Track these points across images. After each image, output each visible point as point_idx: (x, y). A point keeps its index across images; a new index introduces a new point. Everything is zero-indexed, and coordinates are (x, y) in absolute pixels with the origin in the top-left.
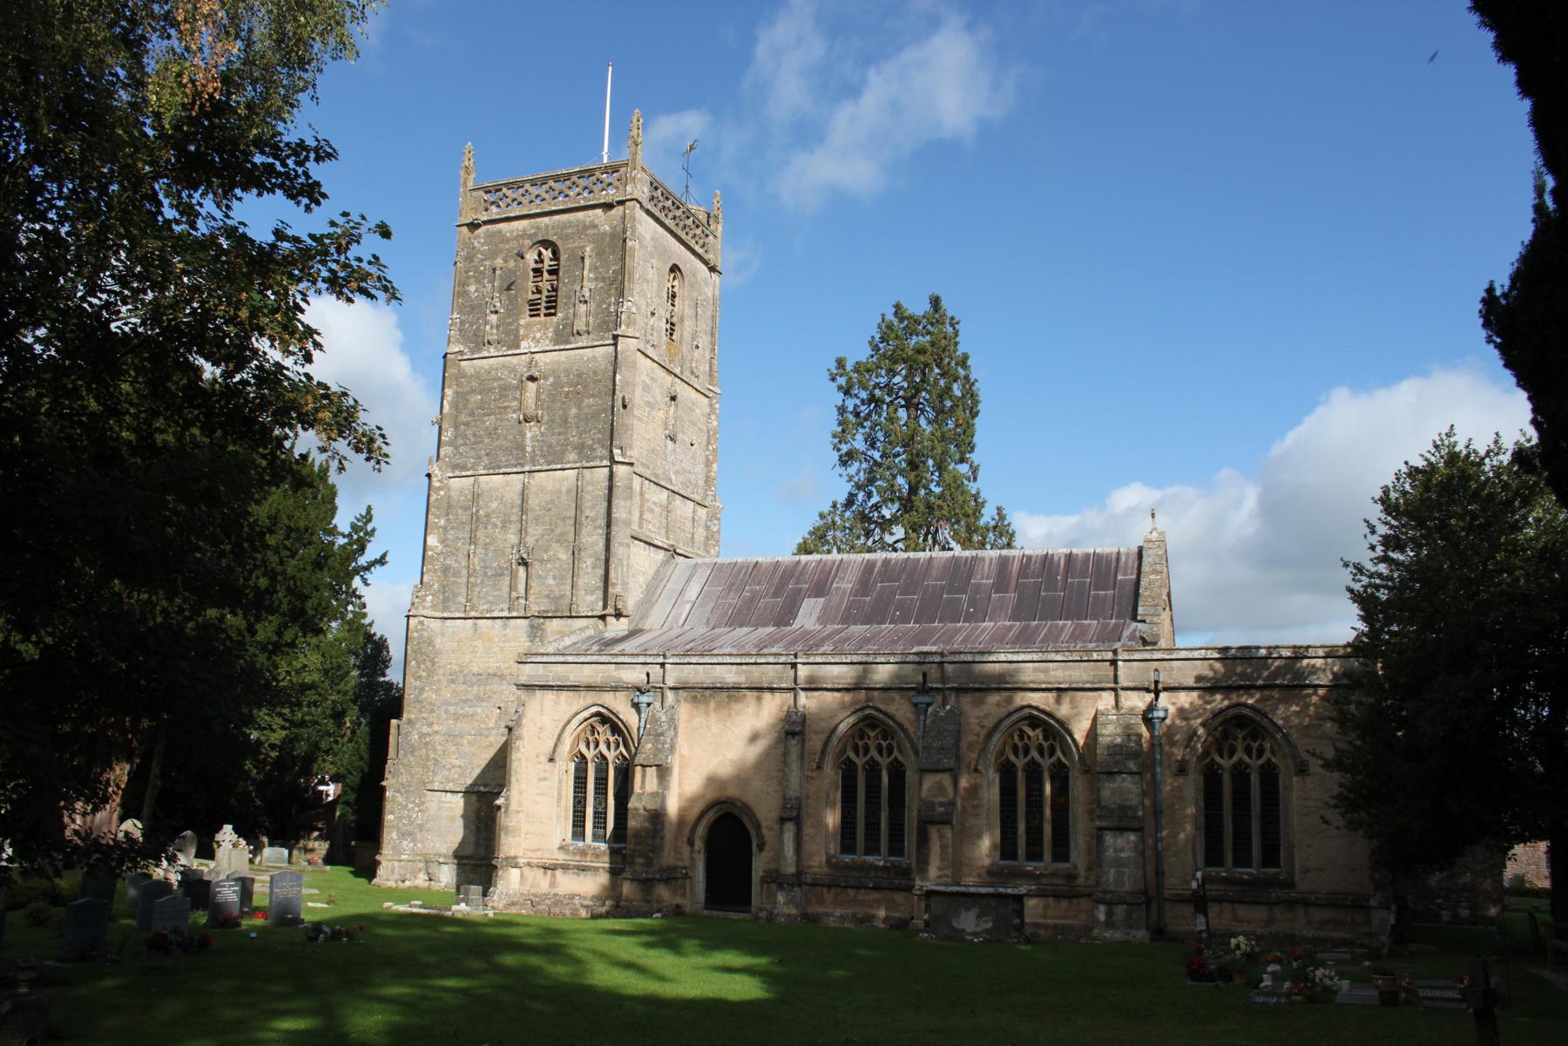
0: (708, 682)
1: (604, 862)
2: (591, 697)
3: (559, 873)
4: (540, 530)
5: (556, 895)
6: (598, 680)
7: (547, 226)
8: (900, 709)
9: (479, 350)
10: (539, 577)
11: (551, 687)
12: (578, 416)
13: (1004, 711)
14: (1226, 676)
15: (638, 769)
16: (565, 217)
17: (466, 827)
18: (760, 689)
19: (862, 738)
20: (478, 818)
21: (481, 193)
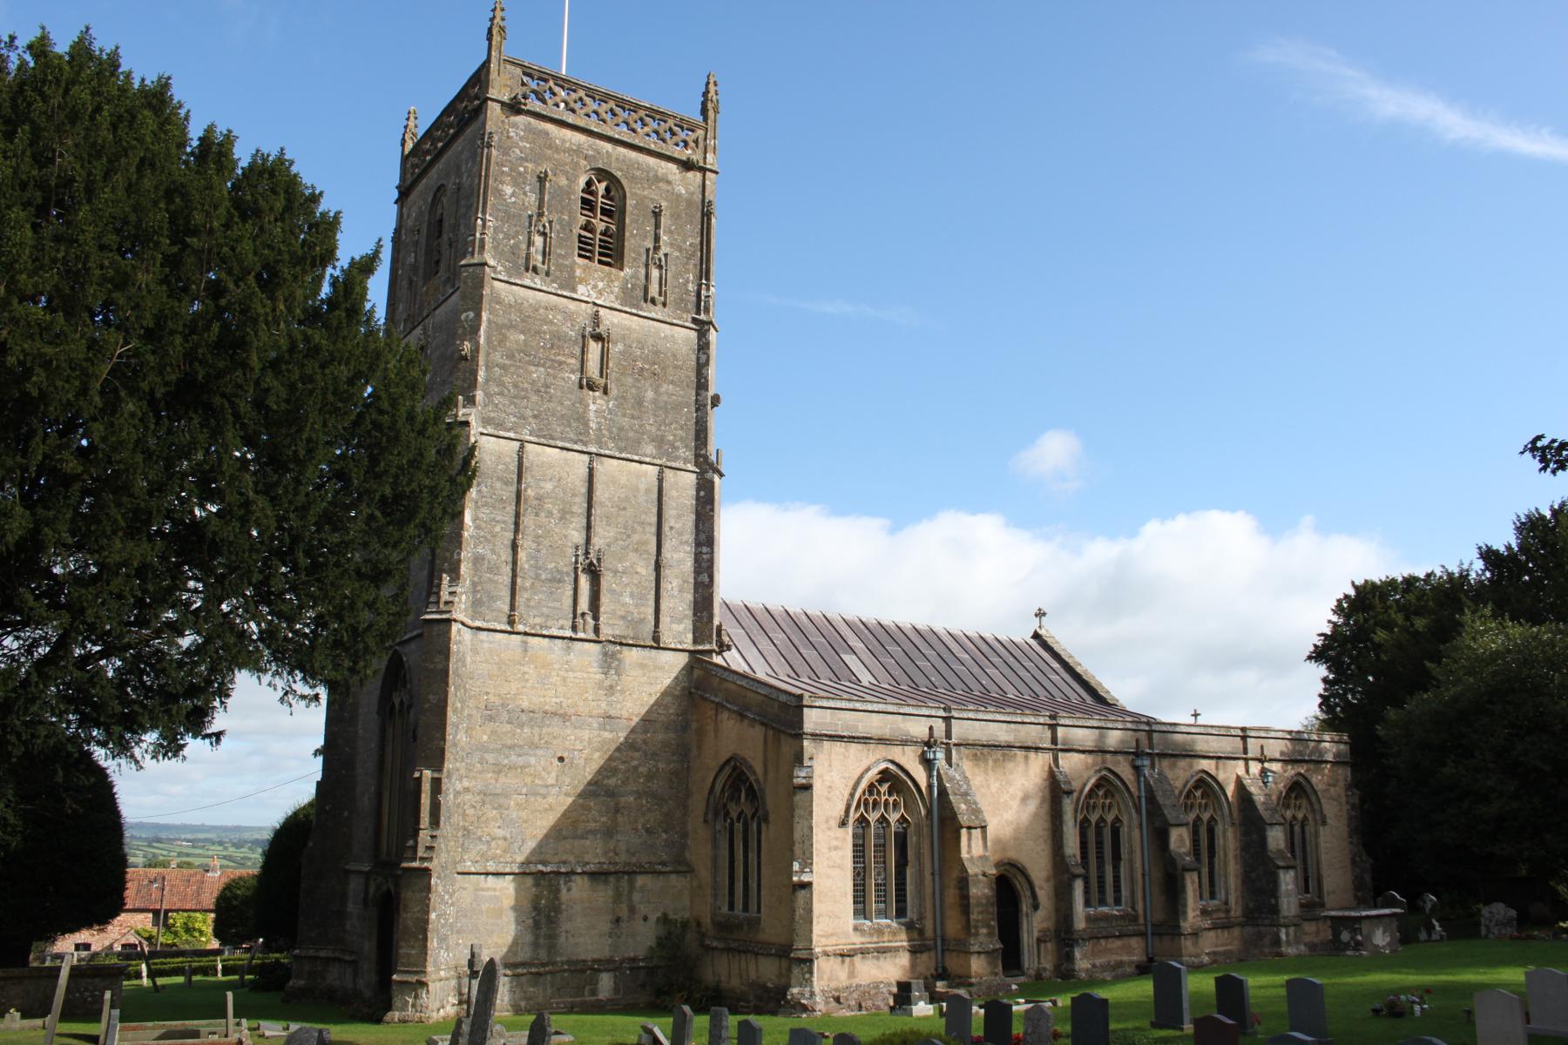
0: (984, 739)
1: (902, 940)
3: (857, 959)
5: (858, 986)
6: (886, 732)
8: (1124, 769)
9: (520, 276)
10: (612, 592)
11: (840, 738)
12: (655, 402)
13: (1188, 774)
14: (1294, 751)
15: (964, 831)
17: (518, 922)
18: (1028, 748)
19: (871, 793)
20: (536, 908)
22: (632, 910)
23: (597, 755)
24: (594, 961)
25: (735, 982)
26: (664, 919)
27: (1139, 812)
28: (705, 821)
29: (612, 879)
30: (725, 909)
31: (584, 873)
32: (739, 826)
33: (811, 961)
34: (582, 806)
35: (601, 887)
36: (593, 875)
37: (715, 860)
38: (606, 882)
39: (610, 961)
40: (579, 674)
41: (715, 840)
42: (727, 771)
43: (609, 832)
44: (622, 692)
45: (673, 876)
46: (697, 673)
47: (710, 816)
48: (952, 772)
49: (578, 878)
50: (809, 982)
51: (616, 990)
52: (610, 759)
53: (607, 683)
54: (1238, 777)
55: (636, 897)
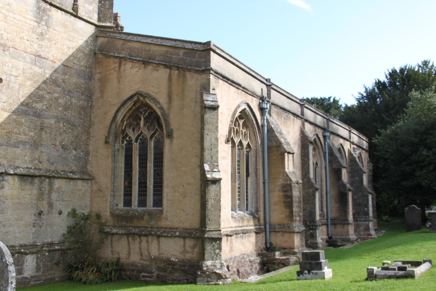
5: (235, 257)
15: (286, 154)
22: (51, 205)
23: (29, 83)
24: (21, 246)
25: (135, 258)
26: (73, 213)
27: (325, 160)
28: (107, 142)
29: (37, 181)
30: (121, 205)
31: (15, 174)
32: (136, 146)
33: (220, 239)
34: (15, 121)
35: (28, 187)
36: (22, 176)
37: (114, 170)
38: (32, 183)
39: (34, 245)
40: (17, 17)
41: (114, 156)
42: (130, 104)
43: (35, 145)
44: (50, 40)
45: (80, 182)
46: (101, 40)
47: (111, 139)
48: (271, 118)
49: (10, 178)
50: (218, 255)
51: (38, 268)
52: (38, 88)
53: (39, 30)
54: (349, 150)
55: (54, 196)
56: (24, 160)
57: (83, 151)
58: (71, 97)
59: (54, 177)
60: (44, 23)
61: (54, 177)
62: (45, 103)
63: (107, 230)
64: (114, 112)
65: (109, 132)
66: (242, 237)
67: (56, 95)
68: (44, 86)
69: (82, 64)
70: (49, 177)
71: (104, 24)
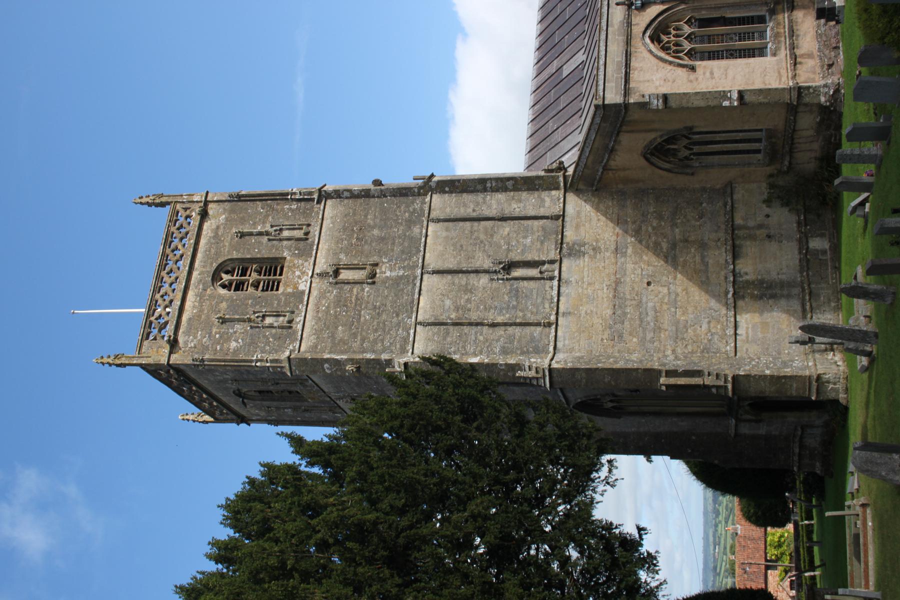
2: (637, 42)
3: (798, 52)
4: (479, 255)
5: (819, 50)
6: (622, 39)
7: (201, 273)
9: (295, 332)
10: (523, 252)
12: (381, 228)
16: (199, 256)
20: (760, 297)
21: (146, 343)
24: (800, 253)
25: (816, 146)
26: (768, 202)
28: (693, 174)
29: (737, 242)
30: (759, 156)
31: (733, 263)
32: (696, 149)
33: (800, 88)
34: (683, 267)
36: (735, 257)
38: (740, 247)
39: (800, 241)
40: (585, 274)
41: (706, 167)
42: (654, 160)
43: (703, 246)
44: (597, 241)
45: (735, 197)
47: (689, 171)
49: (737, 268)
50: (816, 89)
51: (822, 236)
52: (648, 247)
55: (751, 223)
56: (719, 256)
57: (702, 195)
58: (648, 213)
59: (732, 225)
60: (582, 249)
61: (732, 225)
62: (660, 240)
63: (785, 168)
64: (660, 171)
65: (681, 173)
66: (798, 36)
67: (650, 229)
68: (644, 243)
69: (610, 204)
70: (733, 230)
71: (562, 184)
